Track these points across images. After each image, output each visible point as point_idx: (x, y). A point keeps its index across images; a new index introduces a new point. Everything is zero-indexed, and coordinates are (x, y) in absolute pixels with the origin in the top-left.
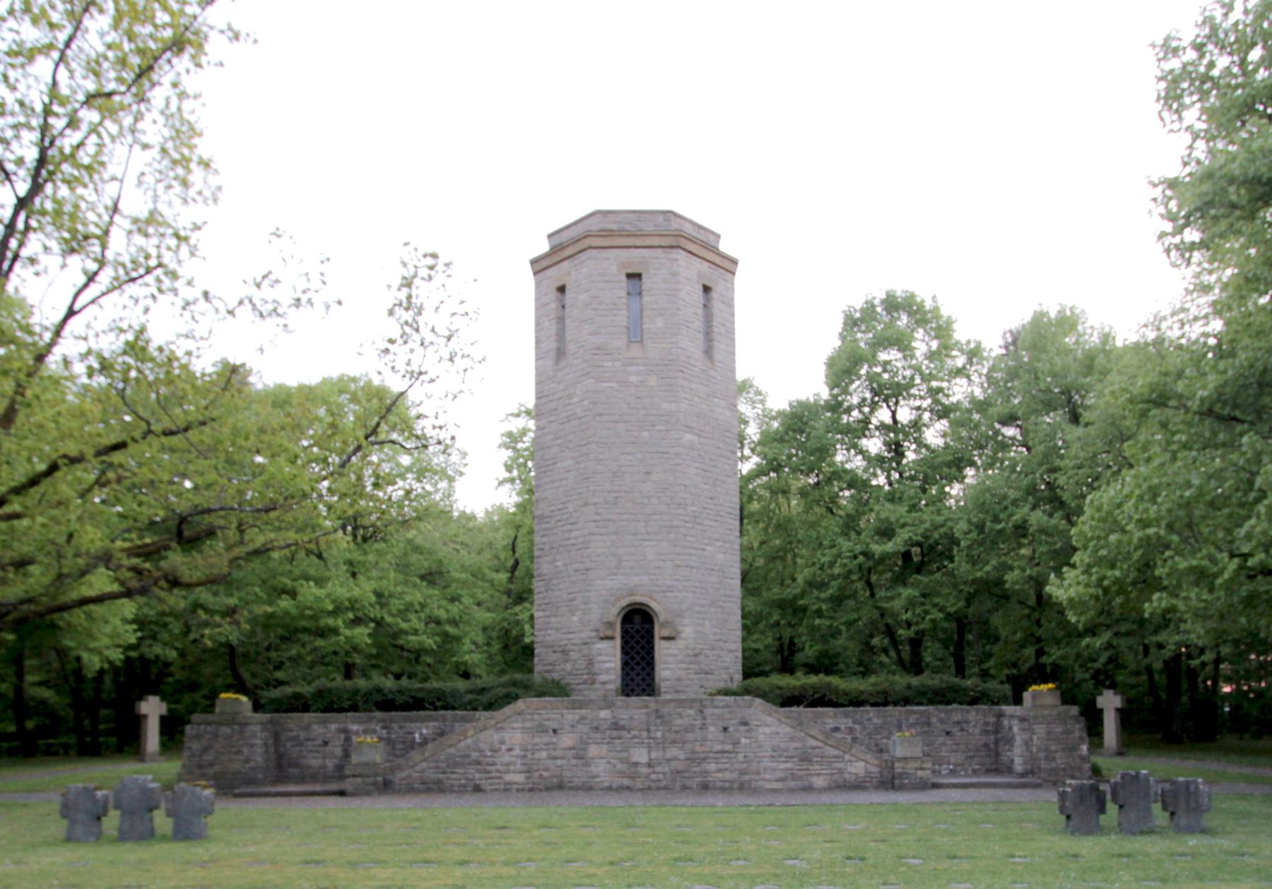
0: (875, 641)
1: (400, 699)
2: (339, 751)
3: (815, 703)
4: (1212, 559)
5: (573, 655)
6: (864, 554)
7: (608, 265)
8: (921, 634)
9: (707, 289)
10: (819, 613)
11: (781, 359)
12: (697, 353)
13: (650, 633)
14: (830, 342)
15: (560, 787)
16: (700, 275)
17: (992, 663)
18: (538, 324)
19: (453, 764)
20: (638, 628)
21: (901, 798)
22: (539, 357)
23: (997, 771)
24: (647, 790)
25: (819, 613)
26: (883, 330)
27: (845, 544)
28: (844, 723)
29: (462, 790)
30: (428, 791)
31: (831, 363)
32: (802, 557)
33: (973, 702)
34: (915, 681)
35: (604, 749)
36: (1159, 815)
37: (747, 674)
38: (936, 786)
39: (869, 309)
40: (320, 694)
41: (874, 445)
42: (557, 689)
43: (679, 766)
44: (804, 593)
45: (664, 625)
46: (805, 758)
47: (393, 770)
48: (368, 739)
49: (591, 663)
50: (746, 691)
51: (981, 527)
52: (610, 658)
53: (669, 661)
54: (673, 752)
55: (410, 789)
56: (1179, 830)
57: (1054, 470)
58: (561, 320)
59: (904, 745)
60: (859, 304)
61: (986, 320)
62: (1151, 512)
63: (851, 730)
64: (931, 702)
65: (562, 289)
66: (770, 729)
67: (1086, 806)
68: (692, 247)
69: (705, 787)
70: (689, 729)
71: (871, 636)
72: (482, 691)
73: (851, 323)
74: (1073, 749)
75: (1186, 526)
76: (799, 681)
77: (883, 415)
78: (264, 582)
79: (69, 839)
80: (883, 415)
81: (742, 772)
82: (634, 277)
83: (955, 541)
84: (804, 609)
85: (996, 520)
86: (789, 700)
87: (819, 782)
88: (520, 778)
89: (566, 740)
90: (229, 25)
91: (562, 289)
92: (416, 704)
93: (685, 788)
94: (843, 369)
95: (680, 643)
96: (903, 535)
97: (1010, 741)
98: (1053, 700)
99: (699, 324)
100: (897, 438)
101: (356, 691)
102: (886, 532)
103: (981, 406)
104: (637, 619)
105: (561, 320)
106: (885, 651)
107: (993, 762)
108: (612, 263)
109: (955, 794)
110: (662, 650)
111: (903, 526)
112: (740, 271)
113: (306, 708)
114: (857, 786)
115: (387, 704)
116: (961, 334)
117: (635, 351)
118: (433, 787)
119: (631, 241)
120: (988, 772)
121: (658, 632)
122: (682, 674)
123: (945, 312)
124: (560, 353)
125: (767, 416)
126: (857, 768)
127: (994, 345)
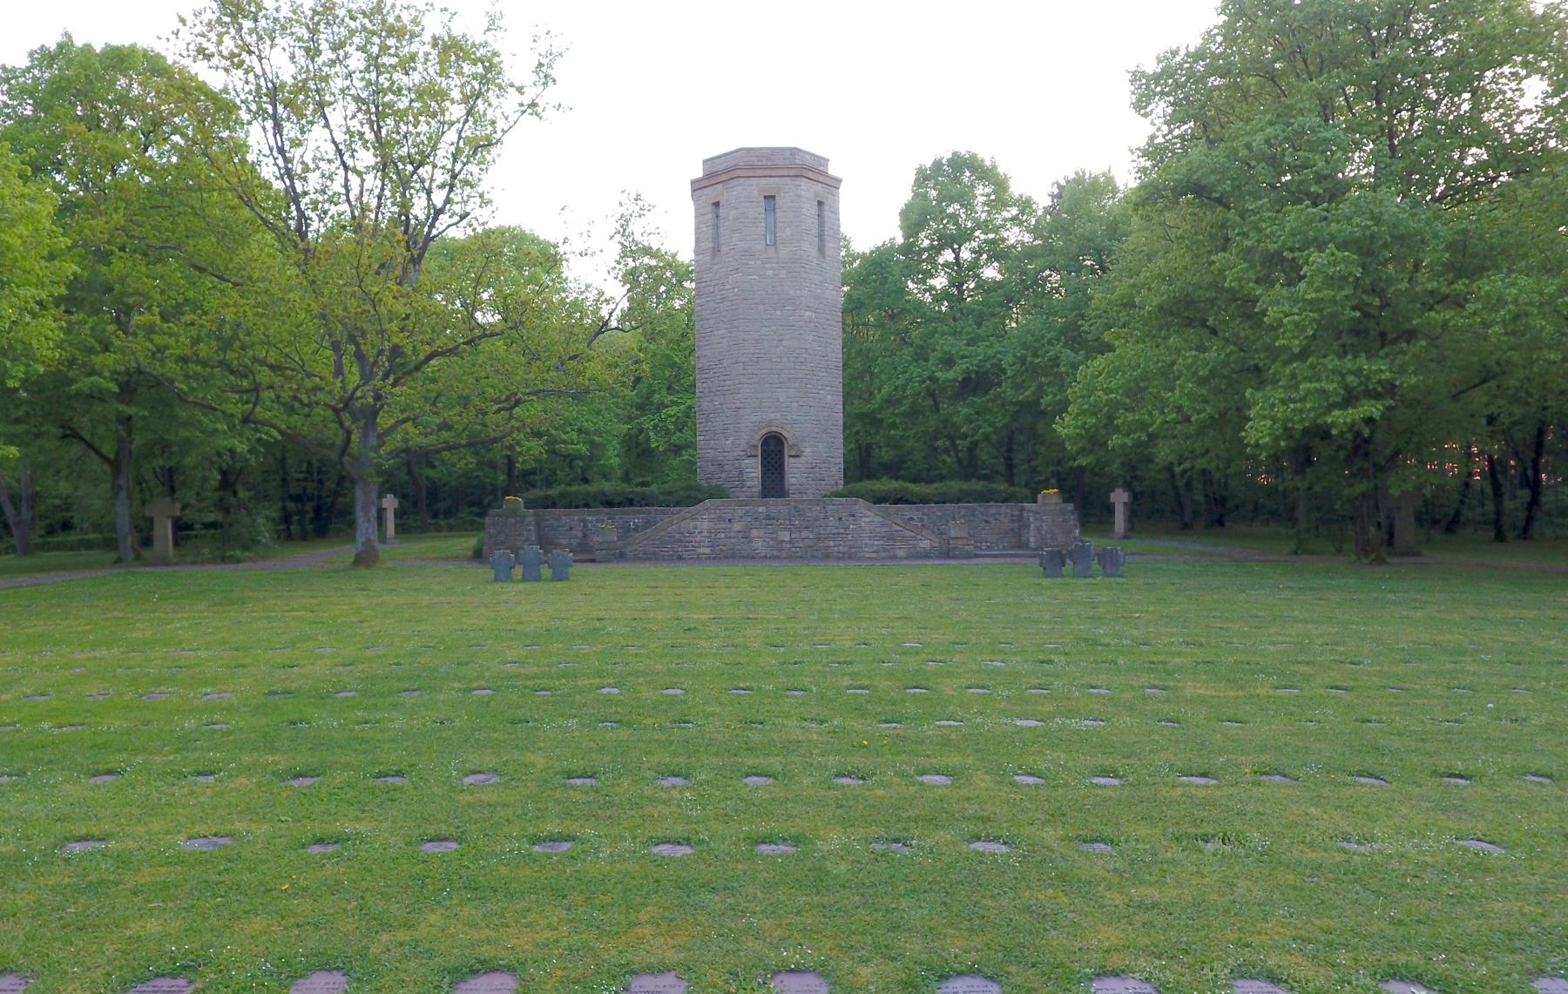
0: (939, 443)
1: (617, 500)
2: (580, 534)
3: (896, 502)
4: (1150, 414)
5: (727, 468)
6: (930, 378)
7: (748, 191)
8: (976, 443)
9: (820, 203)
10: (893, 426)
11: (870, 221)
12: (814, 252)
13: (781, 452)
14: (904, 194)
15: (733, 556)
16: (816, 194)
17: (1039, 461)
18: (697, 228)
20: (773, 449)
21: (954, 562)
23: (1019, 547)
24: (789, 558)
25: (893, 426)
26: (950, 184)
27: (915, 371)
28: (917, 515)
29: (670, 559)
30: (648, 559)
31: (904, 214)
33: (1005, 500)
34: (965, 486)
35: (762, 532)
36: (1095, 565)
37: (848, 477)
38: (977, 556)
40: (562, 496)
41: (940, 282)
42: (718, 493)
43: (810, 543)
44: (881, 409)
45: (791, 447)
47: (625, 546)
48: (604, 526)
49: (741, 473)
50: (850, 494)
51: (1023, 359)
52: (753, 470)
53: (795, 472)
54: (805, 534)
55: (636, 559)
56: (1105, 575)
57: (1082, 317)
58: (716, 227)
59: (955, 530)
60: (928, 164)
61: (1035, 181)
63: (921, 519)
64: (976, 501)
65: (717, 204)
66: (869, 518)
67: (1055, 561)
68: (810, 175)
69: (827, 557)
70: (817, 519)
71: (936, 439)
72: (670, 493)
73: (923, 178)
74: (1070, 532)
75: (1135, 392)
76: (886, 485)
77: (948, 256)
79: (496, 580)
80: (948, 256)
81: (851, 547)
83: (1004, 371)
84: (881, 421)
85: (1035, 355)
86: (880, 499)
87: (901, 553)
88: (707, 551)
89: (737, 526)
90: (651, 207)
91: (717, 204)
93: (814, 557)
94: (914, 219)
95: (803, 460)
97: (1027, 527)
98: (1057, 499)
99: (815, 231)
100: (959, 272)
101: (588, 494)
102: (949, 362)
103: (1030, 253)
104: (772, 442)
105: (716, 227)
106: (947, 451)
107: (1017, 543)
109: (989, 560)
110: (790, 465)
111: (964, 357)
112: (843, 187)
113: (554, 505)
114: (926, 556)
115: (609, 504)
116: (1016, 189)
117: (771, 253)
118: (652, 557)
119: (767, 172)
120: (1013, 547)
122: (803, 480)
123: (1001, 170)
124: (716, 250)
127: (1042, 201)
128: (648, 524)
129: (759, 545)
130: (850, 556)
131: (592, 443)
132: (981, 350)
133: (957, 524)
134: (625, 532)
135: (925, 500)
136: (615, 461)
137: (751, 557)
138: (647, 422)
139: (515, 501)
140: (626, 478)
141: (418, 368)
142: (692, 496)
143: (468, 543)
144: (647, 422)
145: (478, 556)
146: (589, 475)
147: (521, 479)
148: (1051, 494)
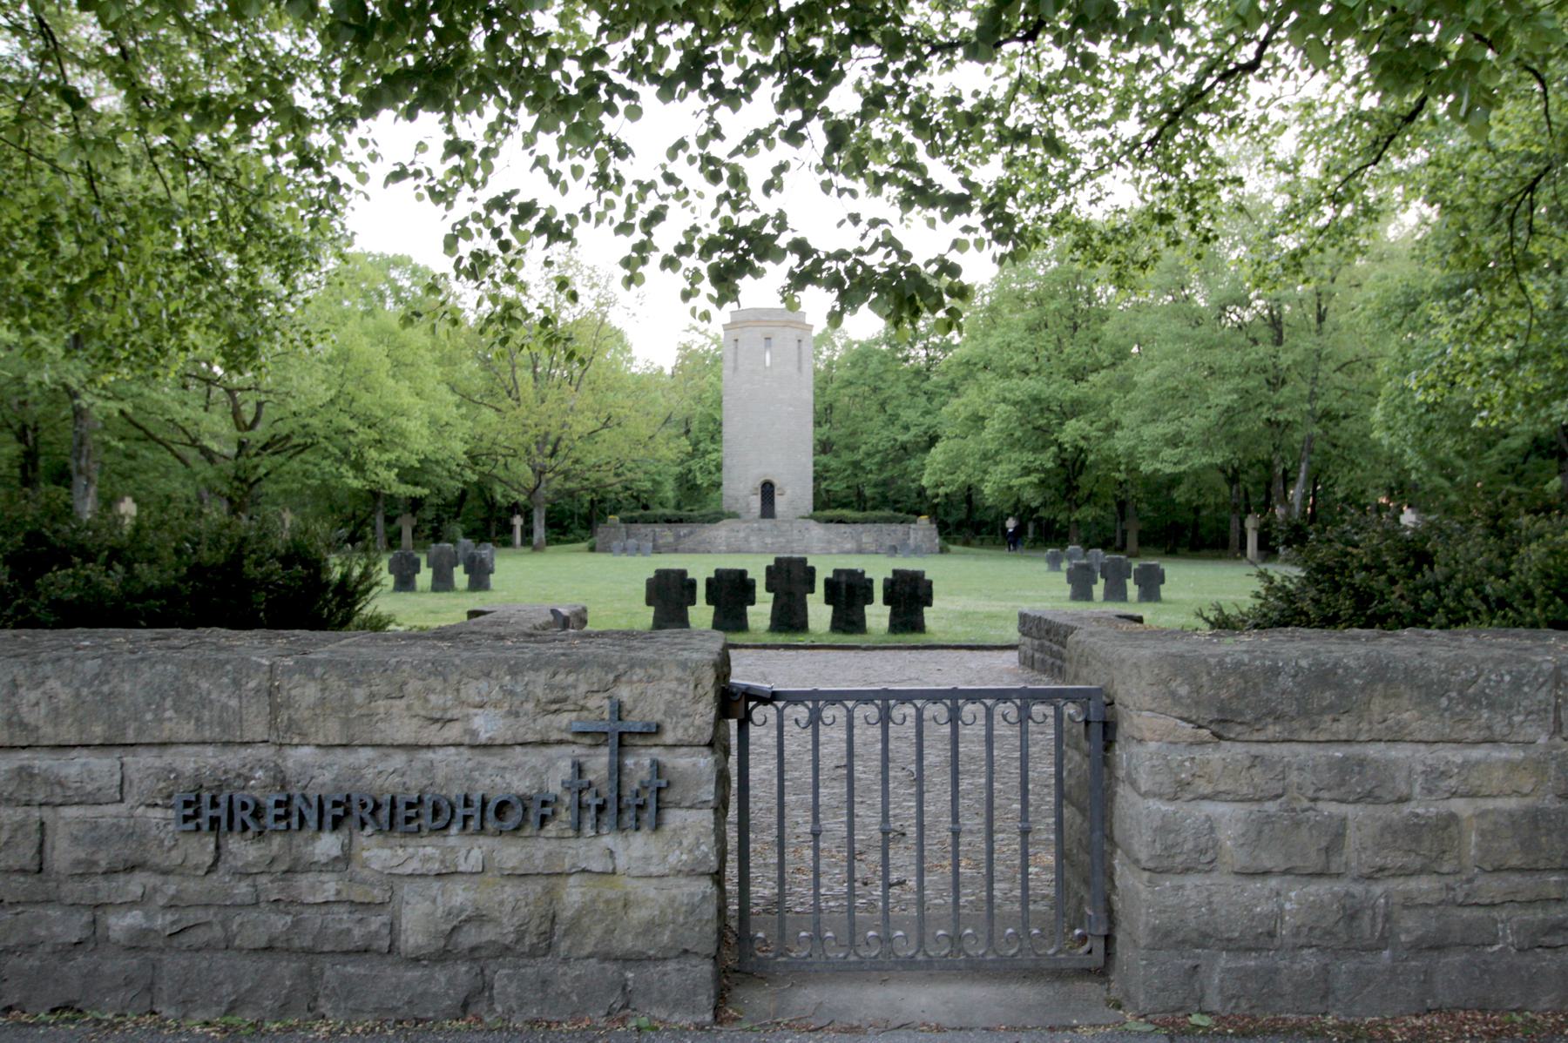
3: (840, 522)
19: (700, 543)
20: (768, 491)
42: (734, 515)
46: (829, 542)
50: (811, 517)
52: (756, 502)
53: (780, 503)
55: (684, 551)
78: (1197, 703)
82: (768, 339)
89: (742, 535)
96: (914, 431)
102: (906, 428)
108: (759, 333)
110: (778, 499)
114: (848, 552)
115: (668, 521)
121: (776, 492)
125: (848, 345)
126: (848, 546)
128: (691, 533)
129: (754, 545)
131: (654, 481)
132: (928, 420)
134: (678, 537)
135: (855, 522)
136: (670, 494)
137: (749, 552)
138: (695, 465)
139: (614, 519)
140: (678, 506)
142: (716, 518)
143: (584, 545)
144: (695, 465)
145: (592, 549)
146: (651, 504)
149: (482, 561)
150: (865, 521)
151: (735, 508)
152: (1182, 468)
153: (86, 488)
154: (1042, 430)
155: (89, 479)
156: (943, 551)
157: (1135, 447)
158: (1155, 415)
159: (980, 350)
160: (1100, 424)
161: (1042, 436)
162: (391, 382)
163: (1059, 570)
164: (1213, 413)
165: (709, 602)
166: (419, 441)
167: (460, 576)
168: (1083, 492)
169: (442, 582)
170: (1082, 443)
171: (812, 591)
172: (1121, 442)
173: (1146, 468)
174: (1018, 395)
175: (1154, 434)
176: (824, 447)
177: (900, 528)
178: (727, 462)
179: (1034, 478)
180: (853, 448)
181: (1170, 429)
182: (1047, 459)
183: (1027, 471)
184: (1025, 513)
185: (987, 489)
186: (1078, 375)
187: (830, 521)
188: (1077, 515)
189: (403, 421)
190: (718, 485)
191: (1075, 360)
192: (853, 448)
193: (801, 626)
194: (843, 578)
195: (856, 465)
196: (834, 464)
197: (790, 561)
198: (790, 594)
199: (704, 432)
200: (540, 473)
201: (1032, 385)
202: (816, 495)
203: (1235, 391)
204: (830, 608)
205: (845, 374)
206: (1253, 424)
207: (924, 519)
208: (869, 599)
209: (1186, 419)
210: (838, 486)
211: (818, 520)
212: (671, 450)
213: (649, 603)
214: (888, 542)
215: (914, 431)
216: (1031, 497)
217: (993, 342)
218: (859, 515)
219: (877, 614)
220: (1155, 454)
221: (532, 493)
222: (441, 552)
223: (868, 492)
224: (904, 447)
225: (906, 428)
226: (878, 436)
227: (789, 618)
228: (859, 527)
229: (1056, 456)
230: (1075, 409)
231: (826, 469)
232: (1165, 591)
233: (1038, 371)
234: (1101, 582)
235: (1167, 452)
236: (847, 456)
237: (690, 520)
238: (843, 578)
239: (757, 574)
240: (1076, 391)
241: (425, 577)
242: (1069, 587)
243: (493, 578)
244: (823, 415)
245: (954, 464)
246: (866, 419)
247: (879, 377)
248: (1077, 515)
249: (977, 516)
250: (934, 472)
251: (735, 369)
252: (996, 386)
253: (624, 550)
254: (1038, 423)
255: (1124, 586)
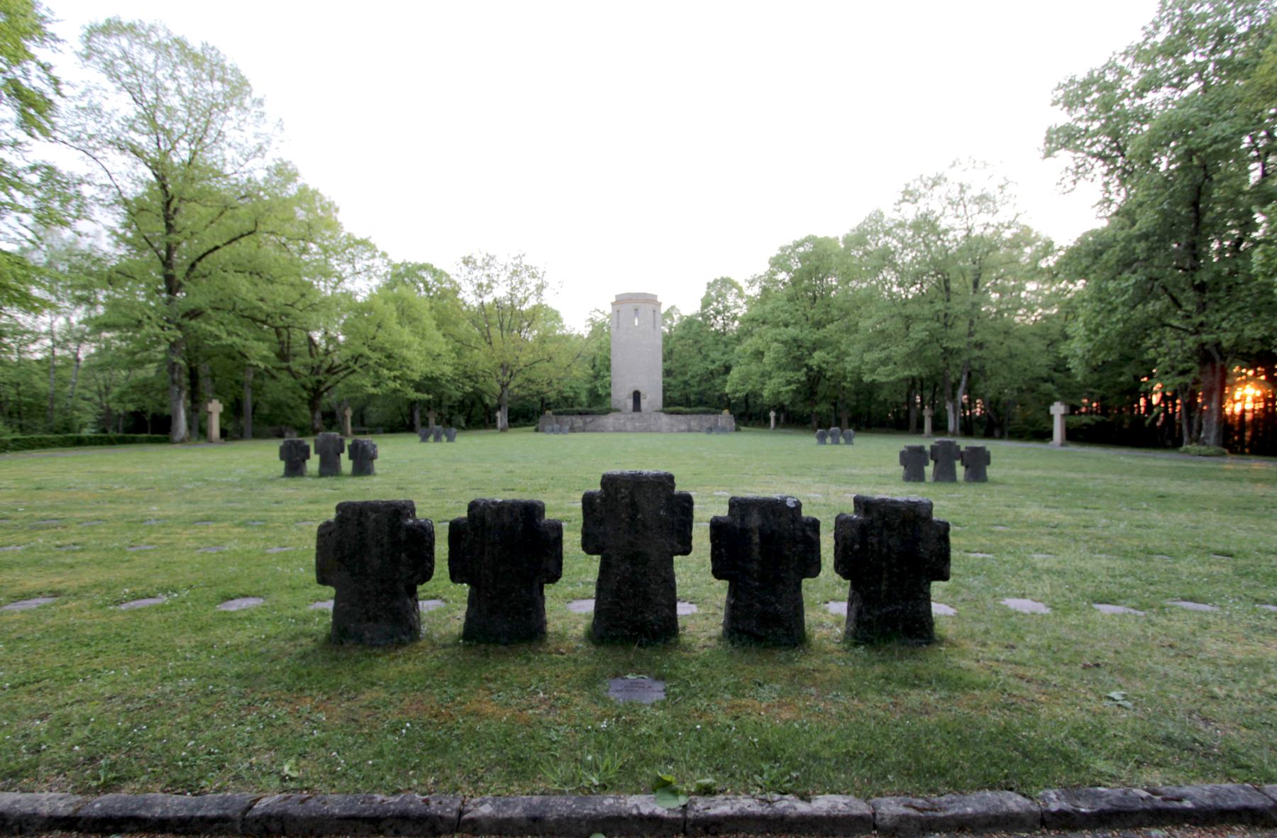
20: (637, 396)
22: (560, 431)
32: (1262, 138)
39: (716, 281)
42: (618, 410)
48: (579, 421)
52: (630, 403)
53: (644, 404)
62: (1138, 251)
66: (665, 419)
92: (587, 413)
94: (706, 303)
96: (718, 363)
110: (643, 401)
126: (683, 427)
130: (659, 431)
132: (726, 357)
133: (694, 421)
134: (585, 423)
135: (686, 413)
137: (626, 431)
138: (598, 383)
139: (548, 412)
140: (589, 406)
141: (1061, 573)
145: (537, 430)
147: (546, 405)
148: (726, 412)
149: (364, 447)
150: (692, 413)
151: (619, 406)
152: (892, 378)
153: (179, 393)
154: (798, 359)
155: (180, 387)
156: (737, 430)
157: (859, 368)
158: (870, 347)
159: (761, 312)
160: (834, 354)
161: (798, 362)
162: (398, 327)
163: (825, 443)
164: (912, 344)
165: (456, 576)
166: (419, 367)
167: (346, 463)
168: (820, 395)
169: (329, 468)
170: (824, 366)
171: (686, 549)
172: (850, 364)
173: (867, 378)
174: (785, 337)
175: (872, 361)
176: (668, 373)
177: (712, 417)
178: (614, 381)
179: (793, 387)
180: (684, 374)
181: (883, 355)
182: (801, 375)
183: (789, 383)
184: (780, 409)
185: (766, 393)
186: (819, 325)
187: (672, 413)
188: (817, 409)
189: (405, 352)
190: (609, 395)
191: (817, 317)
192: (684, 374)
193: (663, 630)
194: (755, 520)
195: (686, 383)
196: (673, 382)
197: (636, 481)
198: (636, 558)
199: (601, 367)
200: (504, 386)
201: (792, 331)
202: (664, 399)
203: (925, 330)
204: (723, 585)
205: (680, 333)
206: (933, 351)
207: (726, 412)
208: (811, 566)
209: (893, 348)
210: (676, 395)
211: (666, 413)
212: (581, 372)
213: (323, 579)
214: (706, 425)
215: (718, 363)
216: (786, 399)
217: (768, 308)
218: (688, 410)
219: (827, 602)
220: (873, 371)
221: (500, 397)
222: (327, 440)
223: (692, 397)
224: (711, 373)
225: (713, 362)
226: (698, 367)
227: (635, 618)
228: (689, 417)
229: (807, 374)
230: (816, 346)
231: (669, 385)
232: (991, 471)
233: (795, 324)
234: (932, 463)
235: (881, 369)
236: (680, 378)
237: (592, 413)
238: (755, 520)
239: (565, 509)
240: (819, 334)
241: (313, 463)
242: (902, 468)
243: (377, 464)
244: (668, 355)
245: (745, 379)
246: (691, 357)
247: (697, 334)
248: (817, 409)
249: (750, 410)
250: (732, 385)
251: (618, 327)
252: (771, 332)
253: (552, 431)
254: (797, 353)
255: (953, 467)
